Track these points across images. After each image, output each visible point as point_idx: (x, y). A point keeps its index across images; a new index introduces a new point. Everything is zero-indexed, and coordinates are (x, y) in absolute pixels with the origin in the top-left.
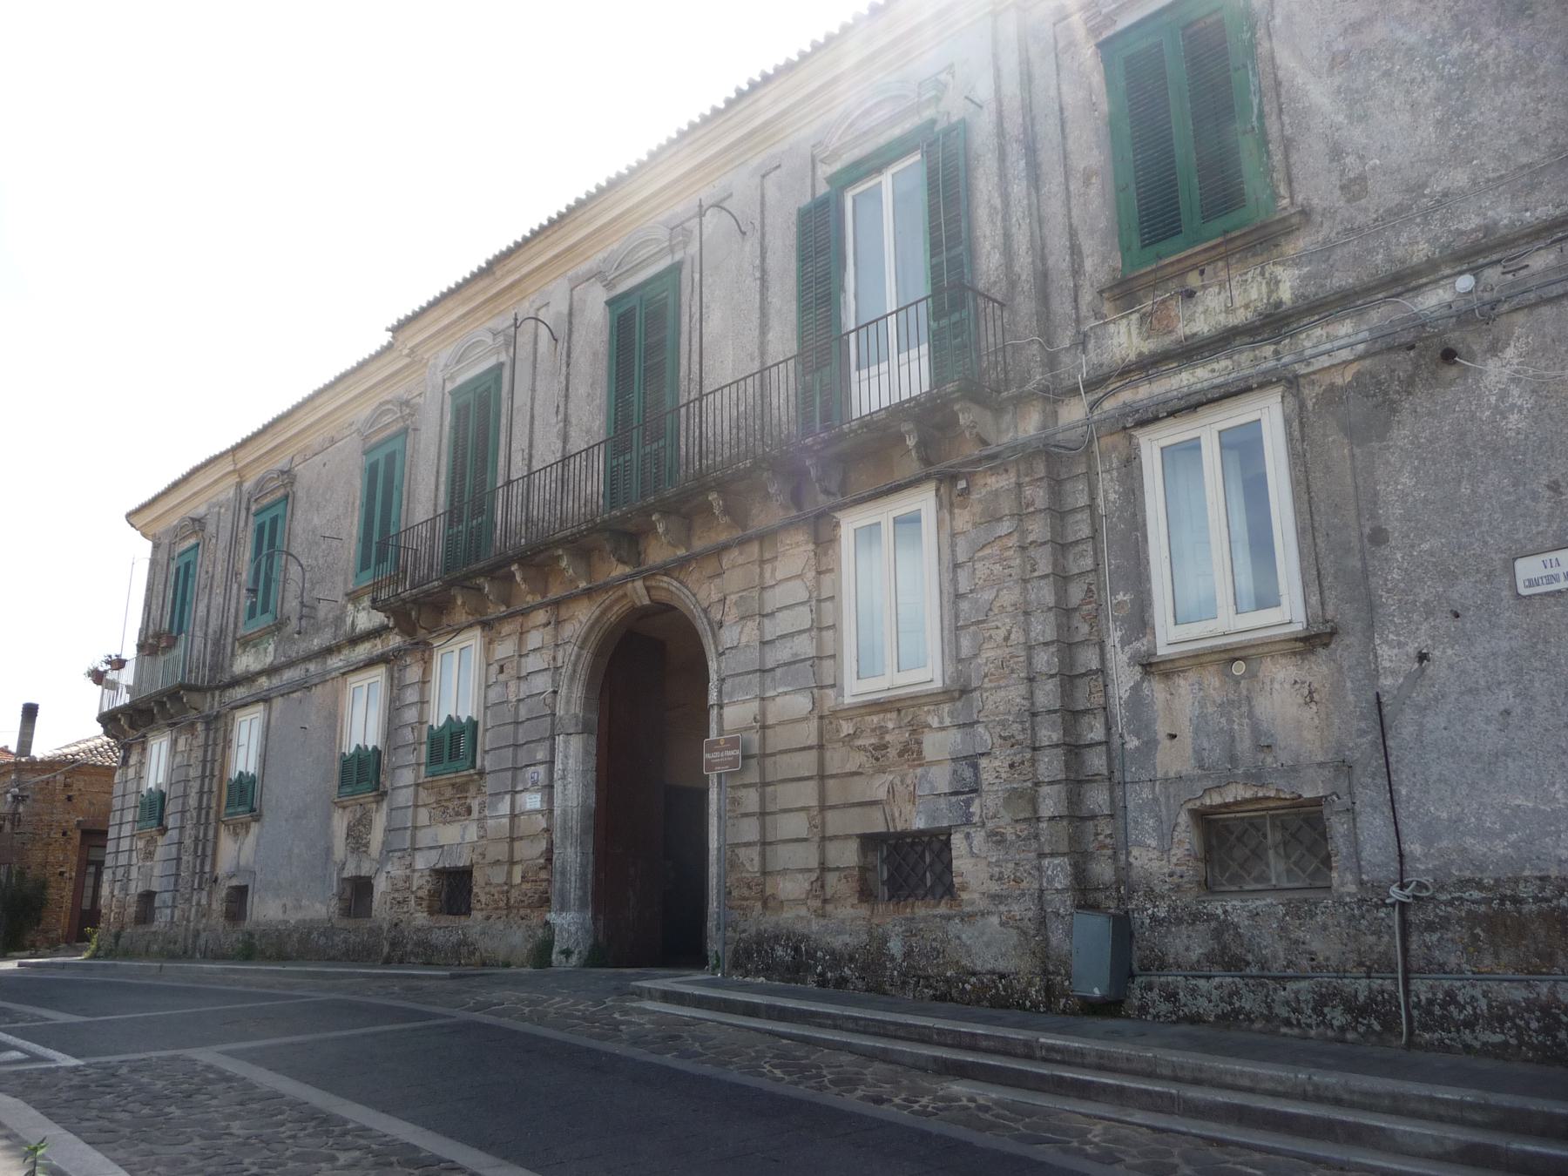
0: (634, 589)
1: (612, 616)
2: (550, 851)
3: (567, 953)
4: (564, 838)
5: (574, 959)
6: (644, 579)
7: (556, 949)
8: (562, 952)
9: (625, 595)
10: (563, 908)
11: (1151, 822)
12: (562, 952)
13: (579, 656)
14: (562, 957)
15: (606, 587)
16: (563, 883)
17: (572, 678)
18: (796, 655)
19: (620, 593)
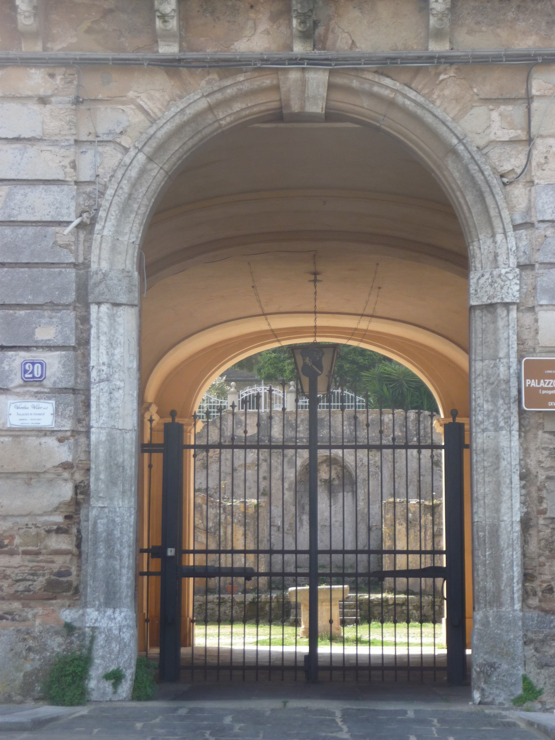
0: (304, 83)
1: (226, 117)
2: (82, 491)
3: (115, 677)
4: (112, 482)
5: (125, 688)
6: (331, 72)
7: (96, 671)
8: (107, 677)
9: (277, 88)
10: (111, 600)
11: (282, 356)
12: (107, 677)
13: (143, 172)
14: (108, 686)
15: (228, 66)
16: (110, 557)
17: (125, 209)
18: (24, 104)
19: (267, 81)
